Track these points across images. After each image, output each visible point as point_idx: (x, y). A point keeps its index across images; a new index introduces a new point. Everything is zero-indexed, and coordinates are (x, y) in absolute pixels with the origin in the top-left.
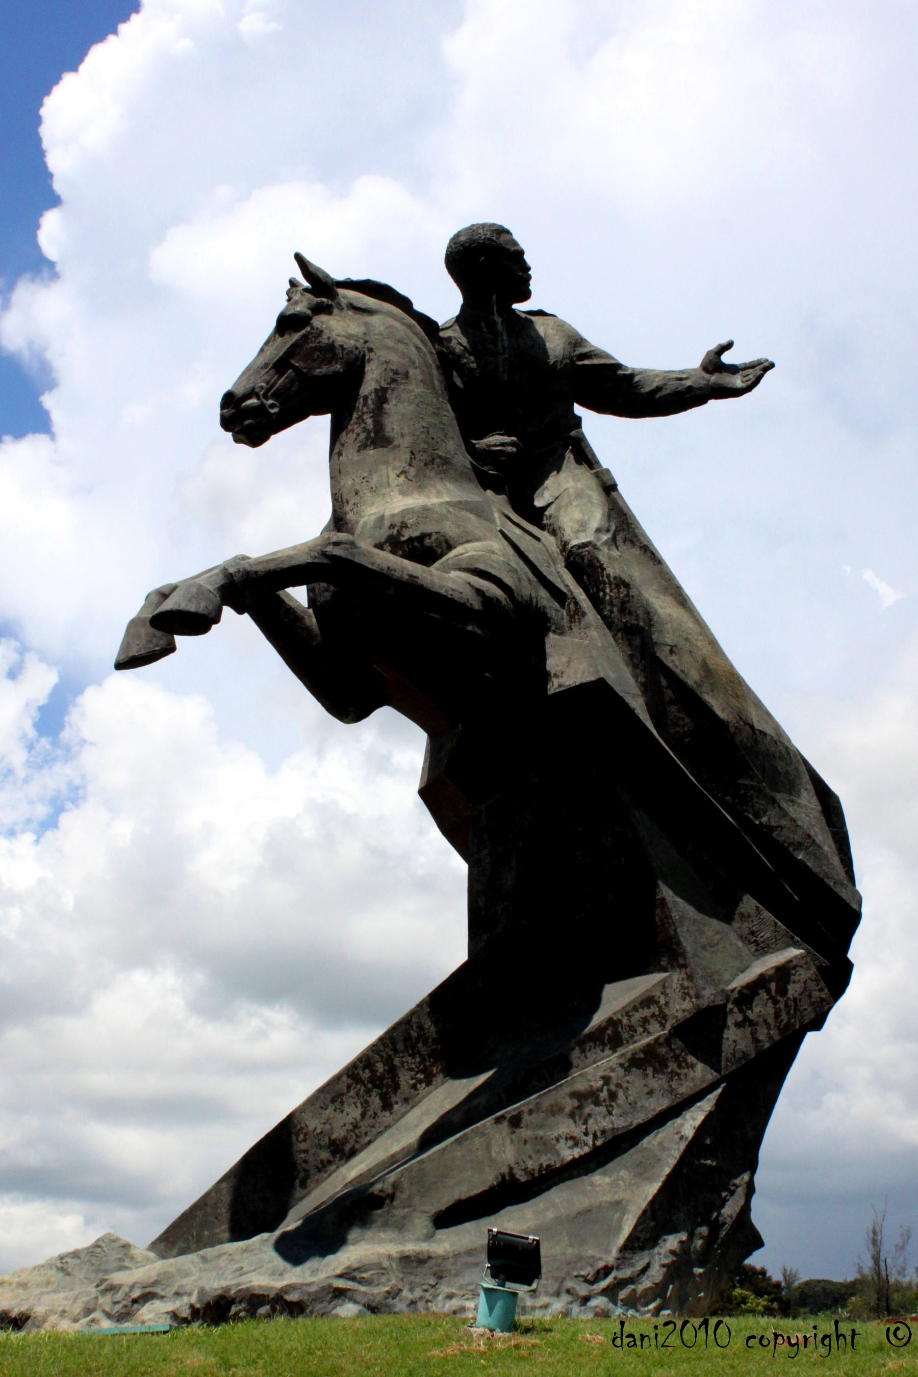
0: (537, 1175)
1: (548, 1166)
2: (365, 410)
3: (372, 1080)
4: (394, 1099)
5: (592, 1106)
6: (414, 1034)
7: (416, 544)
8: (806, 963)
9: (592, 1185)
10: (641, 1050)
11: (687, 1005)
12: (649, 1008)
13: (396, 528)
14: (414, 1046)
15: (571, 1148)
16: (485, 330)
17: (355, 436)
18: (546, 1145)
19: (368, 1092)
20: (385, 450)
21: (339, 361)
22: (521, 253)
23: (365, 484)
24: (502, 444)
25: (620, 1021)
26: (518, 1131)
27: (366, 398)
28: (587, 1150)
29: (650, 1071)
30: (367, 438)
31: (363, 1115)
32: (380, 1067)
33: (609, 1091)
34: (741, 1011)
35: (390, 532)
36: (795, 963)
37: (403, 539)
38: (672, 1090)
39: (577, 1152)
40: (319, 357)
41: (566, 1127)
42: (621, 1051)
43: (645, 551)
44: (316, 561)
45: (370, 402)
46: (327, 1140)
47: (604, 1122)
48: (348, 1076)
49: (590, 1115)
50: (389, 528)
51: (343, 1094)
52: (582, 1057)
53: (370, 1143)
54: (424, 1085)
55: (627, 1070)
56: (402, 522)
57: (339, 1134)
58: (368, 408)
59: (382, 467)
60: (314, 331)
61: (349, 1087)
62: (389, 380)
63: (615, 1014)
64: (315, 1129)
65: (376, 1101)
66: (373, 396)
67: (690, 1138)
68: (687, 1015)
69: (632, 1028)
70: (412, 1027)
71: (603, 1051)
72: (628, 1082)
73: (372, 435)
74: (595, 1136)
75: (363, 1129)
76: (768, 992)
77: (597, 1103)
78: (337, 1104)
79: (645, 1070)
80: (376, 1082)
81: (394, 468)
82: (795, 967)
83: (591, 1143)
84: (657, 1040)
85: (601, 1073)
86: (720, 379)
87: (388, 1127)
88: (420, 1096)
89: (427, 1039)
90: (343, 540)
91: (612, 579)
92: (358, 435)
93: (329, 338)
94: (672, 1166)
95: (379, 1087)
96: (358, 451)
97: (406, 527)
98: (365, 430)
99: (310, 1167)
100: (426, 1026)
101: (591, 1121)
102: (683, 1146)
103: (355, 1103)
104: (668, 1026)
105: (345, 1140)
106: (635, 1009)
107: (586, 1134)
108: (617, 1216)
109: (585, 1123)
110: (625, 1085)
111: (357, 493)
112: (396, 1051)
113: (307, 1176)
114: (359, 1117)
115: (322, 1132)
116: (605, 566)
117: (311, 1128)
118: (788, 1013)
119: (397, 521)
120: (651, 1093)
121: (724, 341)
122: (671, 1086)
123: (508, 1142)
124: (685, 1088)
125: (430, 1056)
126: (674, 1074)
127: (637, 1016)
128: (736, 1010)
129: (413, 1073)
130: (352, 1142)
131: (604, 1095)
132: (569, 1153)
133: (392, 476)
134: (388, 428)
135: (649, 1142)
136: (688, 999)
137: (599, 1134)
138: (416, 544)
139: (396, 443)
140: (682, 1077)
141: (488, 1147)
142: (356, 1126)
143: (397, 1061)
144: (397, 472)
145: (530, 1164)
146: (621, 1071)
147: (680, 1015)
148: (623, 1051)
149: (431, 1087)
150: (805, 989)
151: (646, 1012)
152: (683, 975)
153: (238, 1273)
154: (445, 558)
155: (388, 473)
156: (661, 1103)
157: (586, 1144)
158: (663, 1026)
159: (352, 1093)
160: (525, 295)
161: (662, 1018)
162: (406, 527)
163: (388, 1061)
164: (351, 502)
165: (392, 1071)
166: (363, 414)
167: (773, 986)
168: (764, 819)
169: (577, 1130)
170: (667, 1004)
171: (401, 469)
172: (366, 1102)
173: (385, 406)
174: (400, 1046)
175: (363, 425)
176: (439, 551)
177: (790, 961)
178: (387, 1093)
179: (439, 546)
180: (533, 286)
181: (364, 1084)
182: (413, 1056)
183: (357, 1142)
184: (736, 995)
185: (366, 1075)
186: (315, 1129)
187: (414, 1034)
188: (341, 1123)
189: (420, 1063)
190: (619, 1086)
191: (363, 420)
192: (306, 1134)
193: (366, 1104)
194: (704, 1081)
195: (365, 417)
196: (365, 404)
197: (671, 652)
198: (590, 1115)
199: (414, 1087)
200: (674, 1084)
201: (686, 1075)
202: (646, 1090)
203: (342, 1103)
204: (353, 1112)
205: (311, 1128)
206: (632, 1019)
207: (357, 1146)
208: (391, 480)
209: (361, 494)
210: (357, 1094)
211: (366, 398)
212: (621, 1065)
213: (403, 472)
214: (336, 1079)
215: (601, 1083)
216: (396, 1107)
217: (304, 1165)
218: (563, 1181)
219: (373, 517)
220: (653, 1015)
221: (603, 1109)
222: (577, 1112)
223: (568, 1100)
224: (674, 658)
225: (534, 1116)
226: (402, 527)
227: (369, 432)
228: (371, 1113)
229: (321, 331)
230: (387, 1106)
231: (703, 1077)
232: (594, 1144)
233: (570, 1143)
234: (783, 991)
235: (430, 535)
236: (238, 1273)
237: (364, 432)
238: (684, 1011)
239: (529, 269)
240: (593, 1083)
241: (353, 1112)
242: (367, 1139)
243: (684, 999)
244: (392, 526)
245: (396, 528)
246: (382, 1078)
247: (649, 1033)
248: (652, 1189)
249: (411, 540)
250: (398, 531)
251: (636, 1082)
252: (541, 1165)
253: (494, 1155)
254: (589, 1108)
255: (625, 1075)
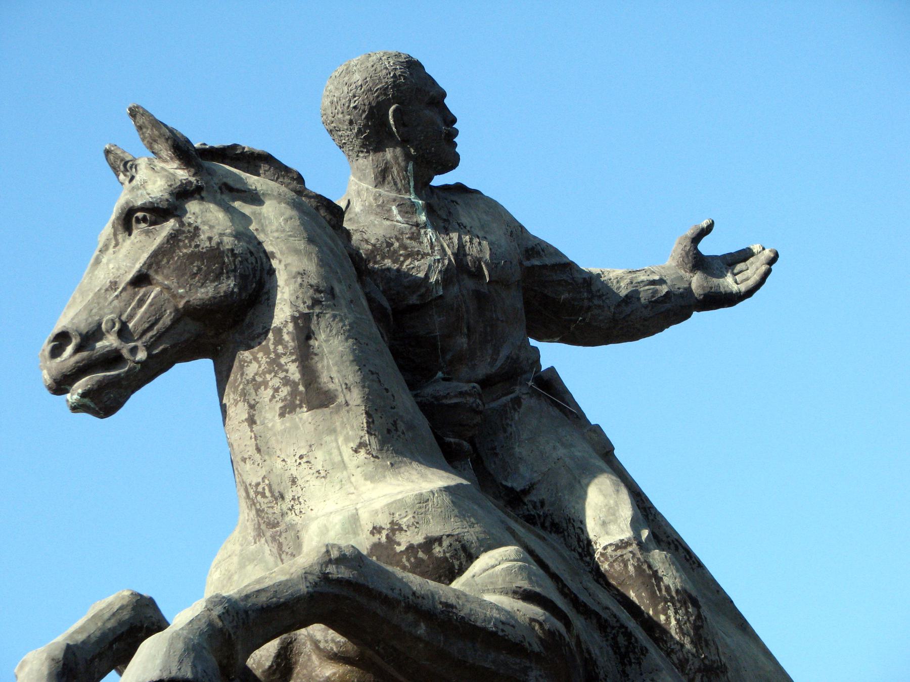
2: (280, 349)
7: (421, 555)
13: (384, 533)
16: (399, 218)
17: (270, 392)
20: (326, 410)
21: (231, 275)
23: (304, 465)
24: (462, 394)
27: (279, 331)
30: (294, 393)
35: (375, 539)
37: (399, 549)
40: (200, 269)
43: (677, 549)
44: (318, 589)
45: (286, 337)
50: (372, 533)
56: (392, 523)
58: (286, 347)
59: (328, 438)
60: (186, 229)
62: (309, 302)
66: (291, 327)
73: (301, 388)
86: (707, 284)
90: (534, 537)
91: (674, 594)
92: (276, 390)
97: (401, 529)
98: (286, 381)
111: (294, 481)
116: (660, 573)
119: (384, 521)
121: (704, 224)
133: (347, 452)
134: (324, 378)
138: (421, 555)
139: (341, 399)
144: (354, 445)
155: (339, 448)
160: (451, 162)
162: (401, 529)
164: (288, 496)
166: (278, 356)
171: (358, 441)
173: (312, 342)
175: (282, 375)
176: (456, 563)
179: (455, 556)
180: (462, 144)
191: (280, 366)
196: (279, 341)
208: (346, 458)
209: (300, 482)
211: (279, 331)
213: (361, 445)
226: (393, 531)
227: (294, 385)
235: (439, 540)
237: (285, 385)
239: (454, 120)
244: (376, 530)
245: (384, 533)
249: (411, 548)
250: (387, 536)
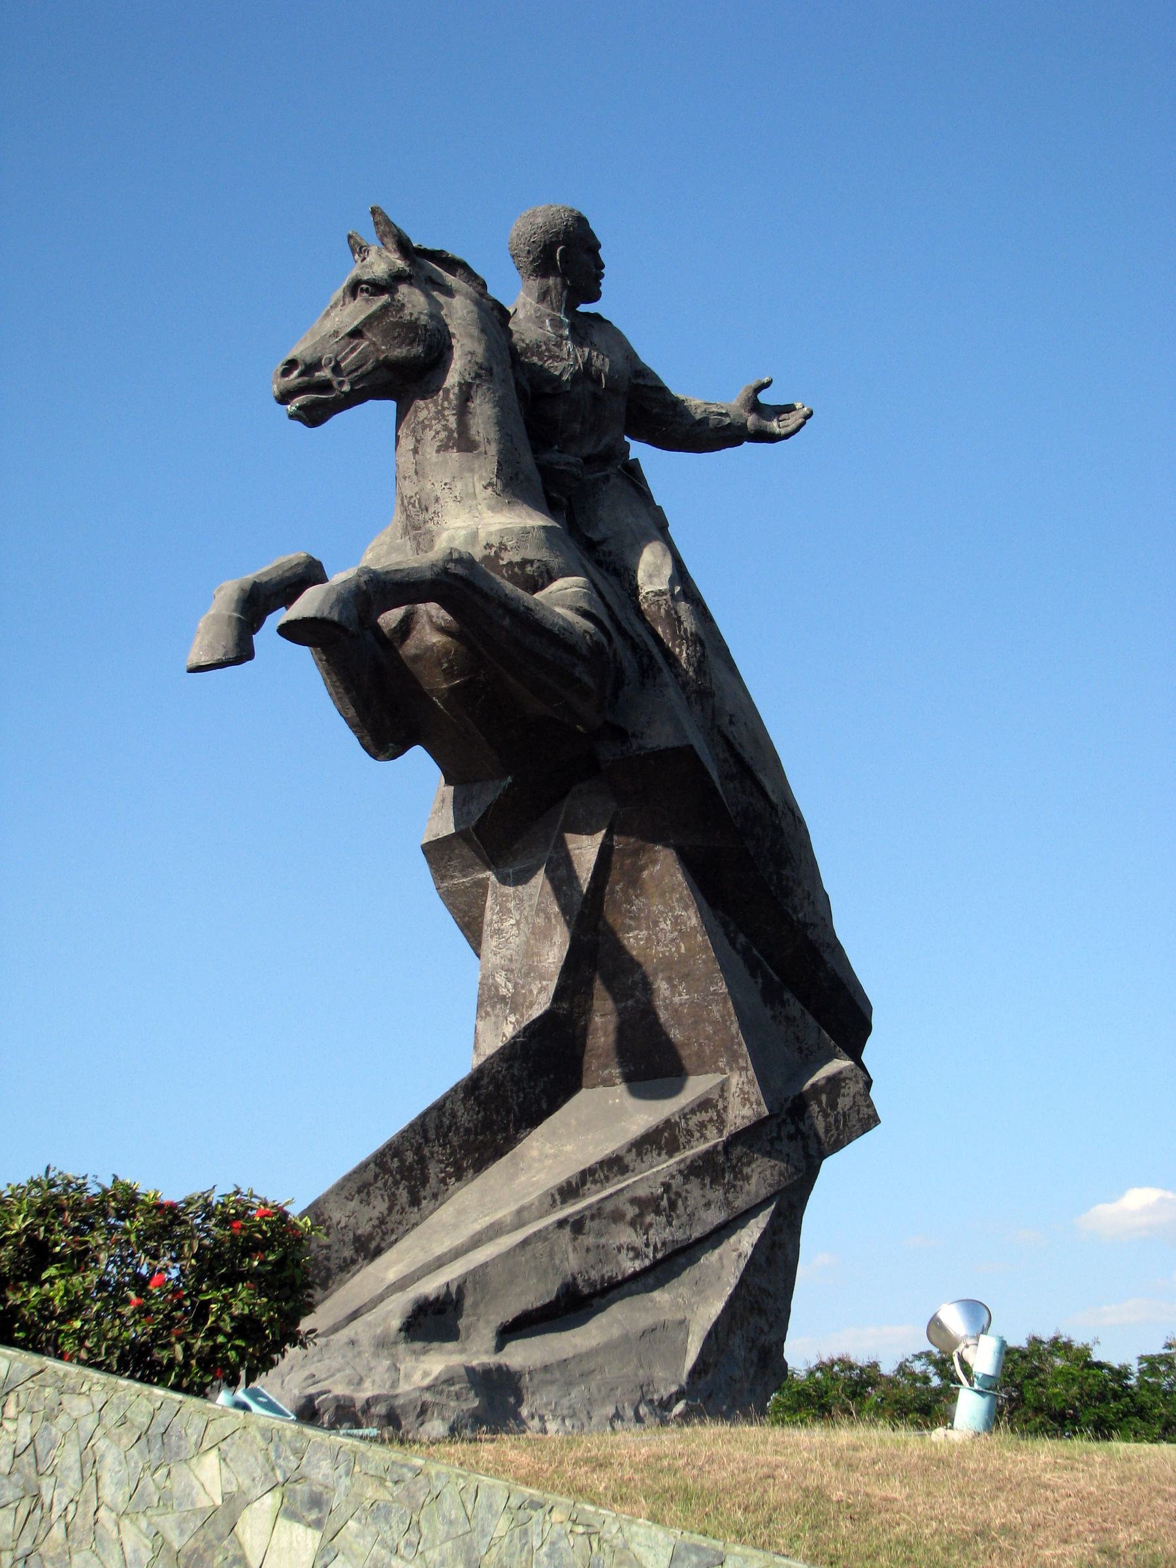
0: (599, 1287)
1: (611, 1278)
3: (400, 1170)
4: (422, 1194)
5: (653, 1215)
6: (446, 1122)
7: (516, 569)
8: (856, 1076)
9: (652, 1301)
10: (699, 1157)
11: (747, 1111)
12: (707, 1112)
13: (494, 549)
14: (446, 1135)
15: (633, 1259)
18: (602, 1253)
19: (396, 1183)
22: (599, 246)
25: (677, 1124)
26: (580, 1237)
28: (647, 1262)
29: (707, 1181)
30: (449, 437)
31: (390, 1209)
32: (410, 1157)
33: (669, 1199)
34: (793, 1123)
36: (844, 1075)
37: (502, 563)
38: (728, 1203)
39: (638, 1265)
41: (627, 1236)
42: (677, 1158)
45: (452, 396)
46: (351, 1236)
47: (663, 1233)
48: (376, 1165)
49: (651, 1225)
51: (370, 1185)
52: (639, 1160)
53: (396, 1241)
54: (453, 1179)
55: (686, 1178)
56: (501, 543)
57: (364, 1229)
58: (450, 403)
61: (376, 1176)
63: (673, 1114)
64: (339, 1223)
65: (403, 1195)
66: (456, 390)
67: (750, 1253)
68: (747, 1123)
69: (690, 1133)
70: (444, 1113)
71: (659, 1155)
72: (687, 1191)
73: (455, 435)
74: (656, 1249)
75: (390, 1226)
76: (820, 1103)
77: (658, 1212)
78: (364, 1195)
79: (703, 1179)
80: (406, 1172)
81: (481, 478)
82: (844, 1079)
83: (651, 1255)
84: (715, 1146)
85: (661, 1179)
87: (415, 1225)
88: (450, 1192)
89: (457, 1129)
92: (437, 433)
93: (411, 314)
94: (734, 1286)
95: (408, 1179)
96: (438, 451)
98: (446, 428)
99: (333, 1265)
100: (459, 1114)
101: (651, 1232)
102: (743, 1264)
103: (382, 1196)
104: (726, 1134)
105: (370, 1237)
106: (693, 1112)
107: (647, 1245)
108: (682, 1336)
109: (646, 1233)
110: (684, 1194)
111: (437, 500)
112: (427, 1140)
113: (329, 1276)
114: (386, 1212)
115: (346, 1227)
117: (335, 1221)
118: (837, 1128)
119: (495, 541)
120: (708, 1205)
122: (726, 1198)
123: (570, 1249)
124: (741, 1203)
125: (461, 1147)
126: (731, 1186)
127: (695, 1120)
128: (788, 1120)
129: (443, 1166)
130: (378, 1239)
131: (664, 1203)
132: (631, 1266)
133: (479, 487)
134: (473, 432)
135: (711, 1258)
136: (748, 1105)
137: (659, 1245)
139: (482, 449)
140: (738, 1189)
141: (552, 1255)
142: (382, 1221)
143: (426, 1151)
144: (484, 483)
145: (594, 1275)
146: (680, 1179)
147: (739, 1121)
148: (682, 1157)
149: (463, 1182)
150: (854, 1103)
151: (704, 1116)
152: (744, 1079)
153: (310, 1381)
154: (547, 591)
156: (715, 1217)
157: (647, 1257)
158: (720, 1132)
159: (380, 1184)
160: (594, 296)
161: (721, 1123)
162: (506, 549)
163: (418, 1150)
164: (431, 510)
165: (422, 1161)
166: (444, 408)
167: (824, 1098)
168: (801, 915)
169: (638, 1241)
170: (725, 1108)
172: (394, 1194)
173: (469, 404)
174: (432, 1135)
175: (443, 423)
177: (840, 1072)
178: (415, 1186)
179: (541, 575)
180: (605, 285)
181: (392, 1175)
182: (444, 1146)
183: (383, 1239)
184: (788, 1104)
185: (395, 1163)
186: (339, 1223)
187: (446, 1122)
188: (367, 1217)
189: (451, 1154)
190: (678, 1194)
191: (444, 416)
192: (329, 1228)
193: (393, 1198)
194: (757, 1196)
195: (446, 413)
196: (446, 398)
197: (731, 722)
198: (651, 1225)
199: (443, 1181)
200: (730, 1196)
201: (741, 1187)
202: (704, 1201)
203: (368, 1194)
204: (380, 1206)
205: (335, 1221)
206: (690, 1122)
207: (383, 1245)
208: (477, 491)
210: (385, 1184)
211: (447, 391)
212: (680, 1172)
214: (364, 1167)
215: (660, 1190)
216: (424, 1203)
217: (326, 1263)
218: (622, 1298)
219: (463, 532)
220: (711, 1120)
221: (663, 1219)
222: (638, 1220)
223: (628, 1206)
224: (733, 729)
225: (597, 1221)
226: (500, 549)
227: (451, 432)
228: (398, 1207)
229: (403, 305)
230: (415, 1201)
231: (757, 1192)
232: (654, 1257)
233: (631, 1254)
234: (833, 1105)
235: (531, 562)
236: (310, 1381)
238: (743, 1117)
239: (603, 267)
240: (653, 1190)
241: (380, 1206)
242: (394, 1237)
243: (744, 1106)
245: (494, 549)
246: (411, 1169)
247: (706, 1138)
248: (716, 1308)
251: (695, 1192)
252: (603, 1276)
253: (557, 1262)
254: (650, 1218)
255: (684, 1184)
